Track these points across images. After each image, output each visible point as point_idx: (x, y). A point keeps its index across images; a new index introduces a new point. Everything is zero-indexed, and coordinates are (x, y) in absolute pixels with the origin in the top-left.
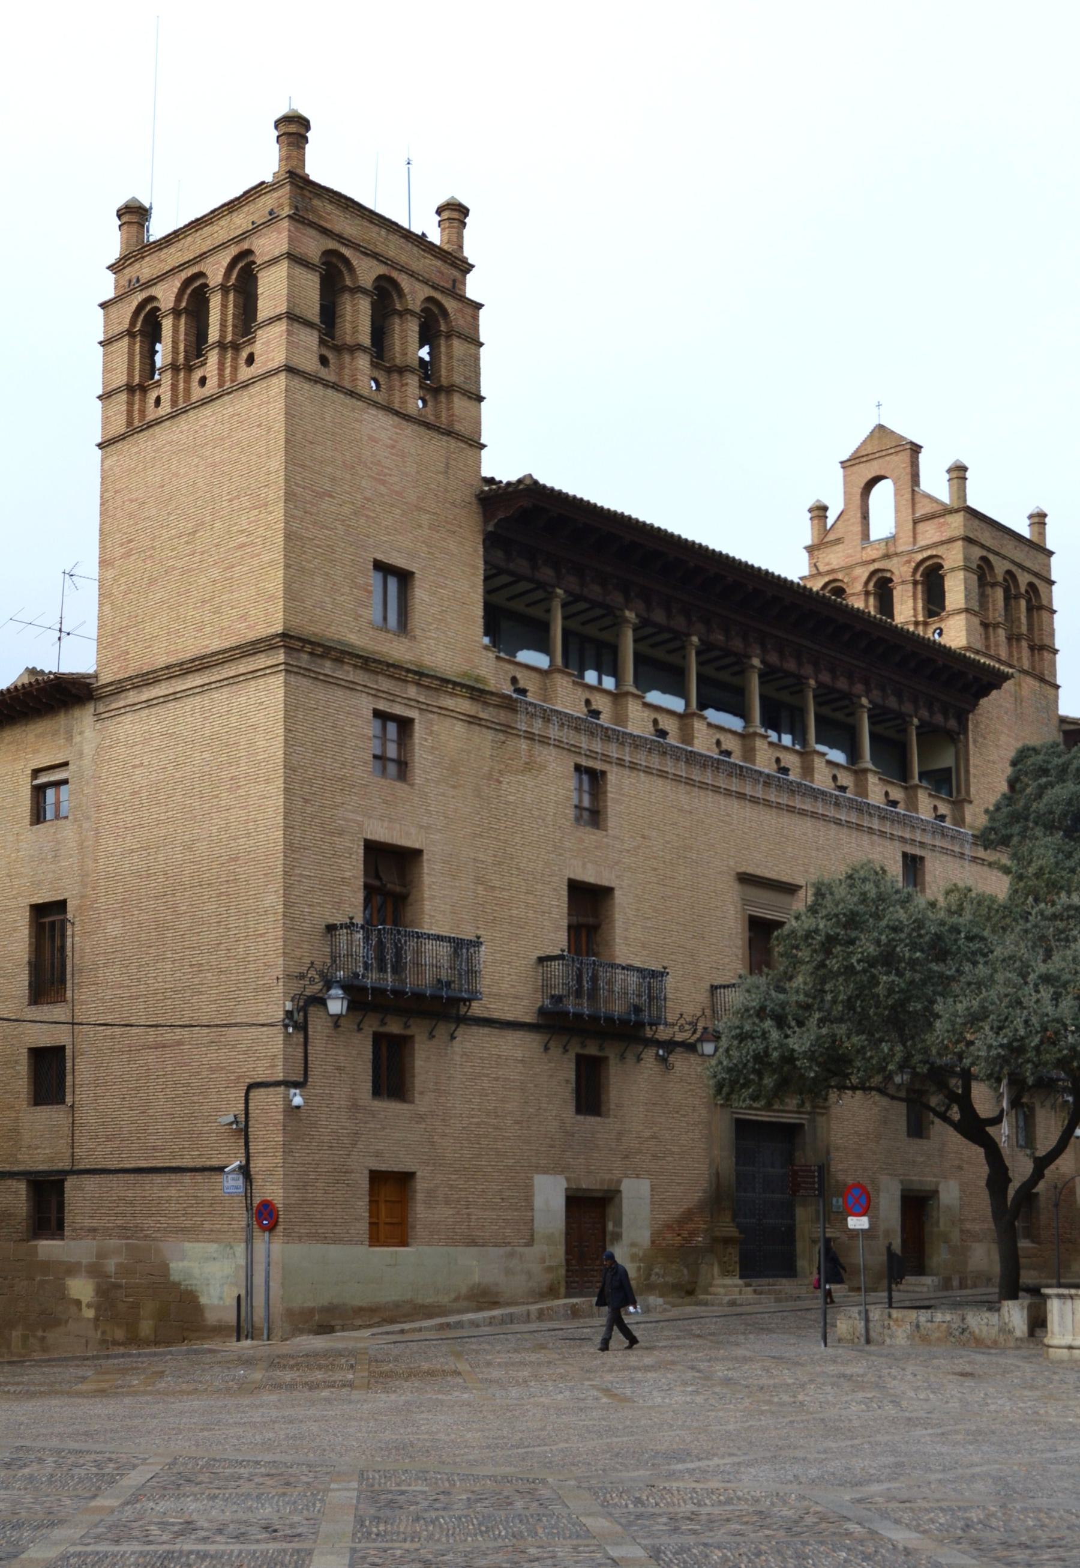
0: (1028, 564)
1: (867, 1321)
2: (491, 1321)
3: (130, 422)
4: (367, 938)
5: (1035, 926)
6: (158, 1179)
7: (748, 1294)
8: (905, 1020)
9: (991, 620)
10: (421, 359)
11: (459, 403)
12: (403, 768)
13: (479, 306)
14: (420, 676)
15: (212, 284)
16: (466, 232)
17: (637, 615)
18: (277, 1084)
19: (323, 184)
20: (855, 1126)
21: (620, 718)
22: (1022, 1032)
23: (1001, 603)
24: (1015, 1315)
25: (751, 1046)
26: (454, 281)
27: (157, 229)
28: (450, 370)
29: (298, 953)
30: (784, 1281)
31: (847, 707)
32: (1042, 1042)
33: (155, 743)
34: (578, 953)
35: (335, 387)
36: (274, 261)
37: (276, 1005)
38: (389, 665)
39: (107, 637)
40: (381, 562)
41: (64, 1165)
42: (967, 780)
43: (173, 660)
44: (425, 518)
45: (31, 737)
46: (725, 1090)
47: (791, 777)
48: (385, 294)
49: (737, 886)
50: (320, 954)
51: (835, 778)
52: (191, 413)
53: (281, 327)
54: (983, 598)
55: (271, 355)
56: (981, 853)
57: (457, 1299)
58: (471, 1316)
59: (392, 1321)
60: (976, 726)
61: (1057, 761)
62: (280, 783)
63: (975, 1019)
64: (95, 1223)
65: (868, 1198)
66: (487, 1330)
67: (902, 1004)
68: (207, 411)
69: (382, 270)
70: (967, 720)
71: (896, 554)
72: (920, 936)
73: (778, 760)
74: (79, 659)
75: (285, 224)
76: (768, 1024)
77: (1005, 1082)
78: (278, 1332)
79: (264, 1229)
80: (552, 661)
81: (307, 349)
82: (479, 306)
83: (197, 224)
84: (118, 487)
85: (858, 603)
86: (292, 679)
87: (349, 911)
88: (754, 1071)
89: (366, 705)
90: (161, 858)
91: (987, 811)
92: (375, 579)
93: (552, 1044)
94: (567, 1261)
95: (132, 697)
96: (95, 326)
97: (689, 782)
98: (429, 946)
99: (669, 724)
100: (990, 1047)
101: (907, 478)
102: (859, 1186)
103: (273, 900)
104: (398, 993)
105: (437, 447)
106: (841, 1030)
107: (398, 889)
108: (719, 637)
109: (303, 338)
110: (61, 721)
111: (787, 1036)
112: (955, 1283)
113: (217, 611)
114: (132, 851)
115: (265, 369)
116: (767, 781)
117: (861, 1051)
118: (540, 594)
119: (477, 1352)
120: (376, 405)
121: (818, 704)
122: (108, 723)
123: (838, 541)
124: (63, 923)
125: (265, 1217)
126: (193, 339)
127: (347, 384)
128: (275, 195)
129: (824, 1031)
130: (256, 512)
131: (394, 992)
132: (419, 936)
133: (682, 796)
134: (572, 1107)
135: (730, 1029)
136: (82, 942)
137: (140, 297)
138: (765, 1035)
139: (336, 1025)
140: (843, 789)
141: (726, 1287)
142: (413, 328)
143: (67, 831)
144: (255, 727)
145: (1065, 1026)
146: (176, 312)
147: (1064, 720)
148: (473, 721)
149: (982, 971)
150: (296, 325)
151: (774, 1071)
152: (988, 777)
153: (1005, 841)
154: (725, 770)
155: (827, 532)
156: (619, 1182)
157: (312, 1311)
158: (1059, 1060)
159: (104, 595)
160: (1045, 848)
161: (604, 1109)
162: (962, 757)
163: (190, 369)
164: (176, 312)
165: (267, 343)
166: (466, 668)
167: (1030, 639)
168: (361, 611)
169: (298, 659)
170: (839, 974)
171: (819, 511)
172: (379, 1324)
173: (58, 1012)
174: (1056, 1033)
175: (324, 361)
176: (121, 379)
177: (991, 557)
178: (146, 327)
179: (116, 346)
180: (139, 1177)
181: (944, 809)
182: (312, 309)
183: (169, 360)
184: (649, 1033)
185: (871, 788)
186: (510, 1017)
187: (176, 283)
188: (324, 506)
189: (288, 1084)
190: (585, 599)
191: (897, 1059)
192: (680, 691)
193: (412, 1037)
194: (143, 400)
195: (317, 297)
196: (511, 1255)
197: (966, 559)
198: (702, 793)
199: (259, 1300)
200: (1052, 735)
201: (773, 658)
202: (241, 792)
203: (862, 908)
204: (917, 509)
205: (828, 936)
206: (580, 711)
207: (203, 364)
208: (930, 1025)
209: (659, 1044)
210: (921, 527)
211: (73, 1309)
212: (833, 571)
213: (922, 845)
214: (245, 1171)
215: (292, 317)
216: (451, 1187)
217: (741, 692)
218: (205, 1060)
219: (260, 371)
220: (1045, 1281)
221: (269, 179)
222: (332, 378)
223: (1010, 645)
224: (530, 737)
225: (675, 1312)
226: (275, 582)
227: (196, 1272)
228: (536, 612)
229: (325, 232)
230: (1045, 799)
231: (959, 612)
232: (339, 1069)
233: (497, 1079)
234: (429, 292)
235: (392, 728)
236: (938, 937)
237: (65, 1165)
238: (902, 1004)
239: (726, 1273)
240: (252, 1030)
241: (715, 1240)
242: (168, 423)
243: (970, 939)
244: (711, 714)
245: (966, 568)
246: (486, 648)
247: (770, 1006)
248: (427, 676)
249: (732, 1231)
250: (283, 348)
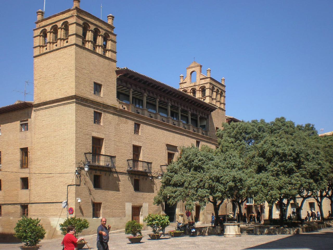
17: (147, 95)
31: (186, 113)
37: (74, 169)
40: (95, 82)
41: (28, 202)
55: (72, 41)
62: (75, 124)
70: (209, 116)
85: (189, 94)
113: (60, 90)
114: (42, 138)
118: (128, 90)
123: (186, 82)
130: (69, 71)
161: (139, 190)
173: (26, 170)
190: (150, 96)
195: (82, 31)
201: (173, 103)
202: (66, 126)
219: (69, 44)
226: (73, 85)
244: (161, 113)
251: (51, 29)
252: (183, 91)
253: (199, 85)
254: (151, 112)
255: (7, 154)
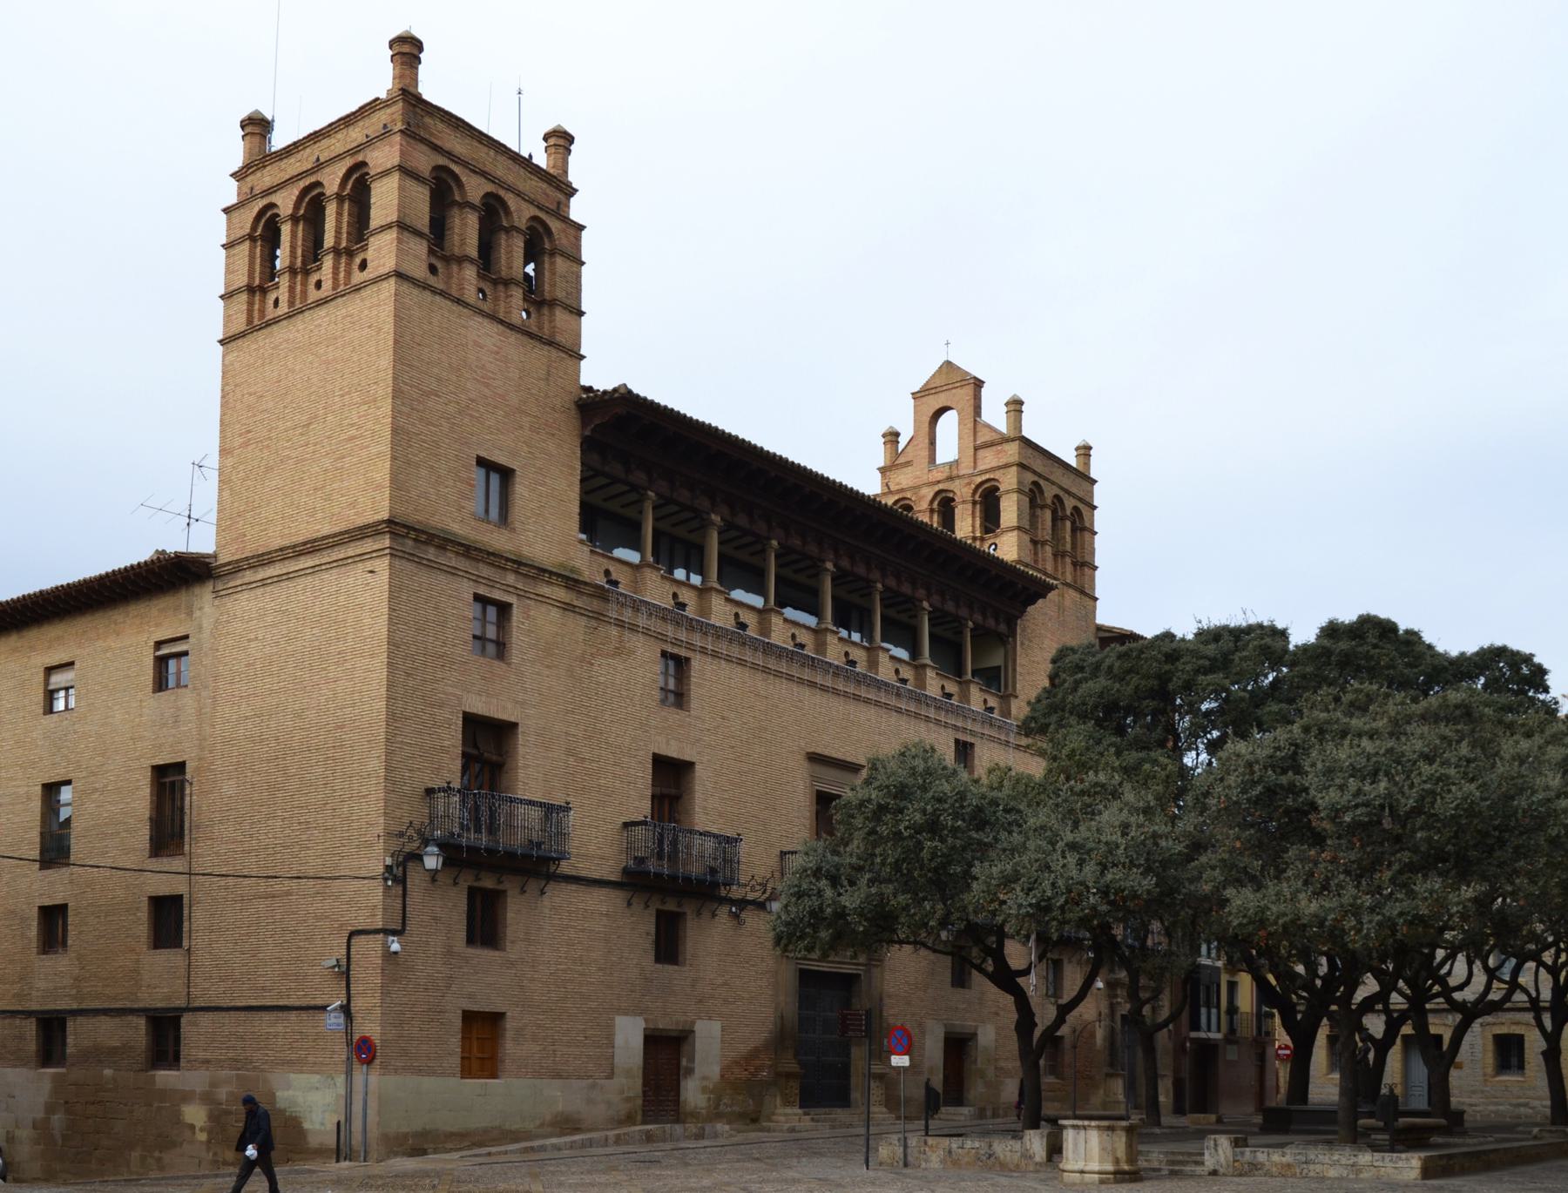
0: (1074, 490)
1: (906, 1147)
2: (572, 1146)
3: (250, 321)
4: (463, 802)
5: (1065, 801)
6: (266, 1016)
7: (807, 1122)
8: (945, 882)
9: (1039, 538)
10: (526, 275)
11: (560, 315)
12: (501, 648)
13: (581, 228)
14: (519, 565)
15: (328, 193)
16: (571, 159)
18: (377, 931)
19: (435, 102)
20: (906, 976)
21: (704, 610)
22: (1049, 894)
23: (1049, 523)
24: (1035, 1142)
25: (807, 903)
26: (559, 203)
27: (280, 139)
28: (553, 285)
29: (398, 814)
30: (839, 1110)
32: (1066, 902)
33: (269, 619)
34: (661, 819)
35: (443, 294)
36: (386, 173)
37: (377, 860)
38: (489, 553)
39: (226, 521)
41: (180, 1002)
42: (1014, 677)
43: (286, 543)
44: (526, 421)
45: (154, 612)
46: (784, 942)
47: (858, 670)
48: (492, 212)
49: (806, 764)
50: (420, 815)
51: (897, 672)
52: (307, 314)
53: (392, 235)
54: (1033, 518)
56: (1024, 741)
57: (542, 1125)
58: (554, 1140)
59: (481, 1145)
60: (1024, 630)
61: (1091, 660)
63: (1008, 881)
64: (208, 1055)
65: (910, 1038)
66: (566, 1152)
67: (944, 866)
68: (322, 311)
69: (489, 188)
71: (958, 477)
72: (962, 807)
73: (847, 654)
74: (202, 542)
75: (397, 138)
76: (824, 883)
77: (1033, 937)
78: (374, 1155)
79: (363, 1062)
80: (643, 557)
81: (416, 256)
82: (581, 228)
83: (315, 137)
84: (238, 381)
85: (925, 518)
86: (397, 562)
87: (447, 776)
88: (810, 925)
89: (467, 589)
90: (273, 724)
91: (1029, 703)
92: (479, 474)
93: (634, 901)
94: (644, 1092)
95: (249, 576)
96: (219, 230)
97: (766, 670)
98: (521, 809)
99: (749, 618)
100: (1020, 906)
101: (971, 410)
102: (902, 1028)
103: (376, 764)
104: (491, 852)
105: (539, 356)
106: (888, 889)
107: (494, 758)
108: (796, 542)
109: (412, 245)
110: (183, 597)
111: (840, 895)
112: (989, 1113)
113: (328, 498)
115: (377, 274)
116: (837, 672)
117: (906, 908)
118: (633, 497)
119: (553, 1173)
120: (481, 313)
121: (884, 606)
122: (226, 600)
123: (908, 464)
124: (183, 782)
125: (364, 1051)
126: (310, 244)
127: (455, 293)
128: (389, 111)
129: (873, 890)
131: (487, 850)
132: (512, 800)
133: (759, 682)
134: (462, 935)
135: (790, 887)
136: (198, 801)
137: (261, 203)
138: (820, 893)
139: (434, 880)
140: (904, 681)
141: (788, 1116)
142: (518, 244)
143: (187, 699)
144: (361, 606)
145: (1088, 888)
146: (294, 219)
147: (1100, 628)
148: (567, 607)
149: (1017, 838)
150: (406, 234)
151: (829, 926)
152: (1032, 674)
153: (1043, 730)
154: (799, 662)
155: (898, 455)
156: (693, 1023)
157: (406, 1136)
158: (1081, 919)
159: (224, 481)
160: (1077, 736)
162: (1011, 657)
163: (307, 273)
164: (294, 219)
165: (379, 250)
166: (562, 559)
167: (1073, 557)
168: (464, 503)
169: (403, 545)
170: (888, 839)
171: (892, 437)
172: (469, 1148)
173: (177, 864)
174: (1080, 895)
175: (433, 269)
176: (242, 280)
177: (1042, 482)
178: (265, 232)
179: (238, 249)
180: (249, 1015)
181: (992, 702)
182: (422, 219)
183: (287, 263)
184: (723, 893)
185: (928, 681)
186: (596, 875)
187: (294, 192)
188: (430, 404)
189: (387, 932)
191: (937, 916)
192: (760, 590)
193: (504, 892)
194: (263, 302)
195: (427, 209)
196: (593, 1086)
197: (1020, 482)
198: (777, 681)
199: (357, 1125)
200: (1089, 637)
201: (845, 563)
202: (348, 665)
203: (911, 781)
204: (978, 438)
205: (879, 805)
206: (668, 603)
207: (319, 268)
208: (969, 886)
209: (732, 902)
210: (981, 453)
211: (188, 1133)
212: (902, 490)
213: (972, 733)
214: (346, 1010)
215: (402, 226)
216: (539, 1026)
217: (815, 593)
218: (311, 910)
220: (1063, 1113)
221: (383, 95)
222: (441, 286)
223: (1055, 560)
224: (620, 624)
225: (739, 1138)
227: (301, 1100)
228: (630, 513)
229: (436, 148)
230: (1080, 691)
231: (1012, 529)
232: (435, 919)
233: (583, 931)
234: (534, 212)
235: (492, 612)
236: (979, 809)
237: (181, 1003)
238: (944, 866)
239: (787, 1103)
240: (355, 882)
241: (778, 1075)
242: (285, 323)
243: (1006, 811)
244: (789, 612)
245: (1019, 491)
246: (581, 542)
247: (826, 867)
248: (526, 565)
249: (793, 1067)
250: (393, 255)
251: (297, 206)
252: (896, 502)
253: (973, 475)
254: (795, 624)
255: (96, 790)
